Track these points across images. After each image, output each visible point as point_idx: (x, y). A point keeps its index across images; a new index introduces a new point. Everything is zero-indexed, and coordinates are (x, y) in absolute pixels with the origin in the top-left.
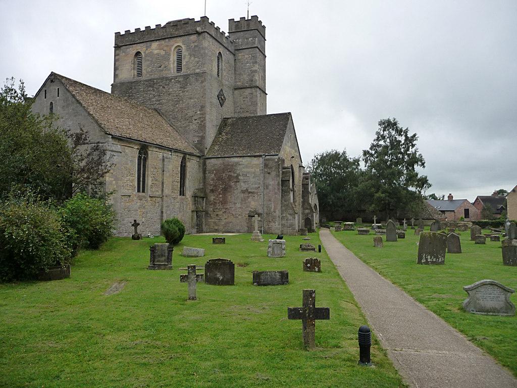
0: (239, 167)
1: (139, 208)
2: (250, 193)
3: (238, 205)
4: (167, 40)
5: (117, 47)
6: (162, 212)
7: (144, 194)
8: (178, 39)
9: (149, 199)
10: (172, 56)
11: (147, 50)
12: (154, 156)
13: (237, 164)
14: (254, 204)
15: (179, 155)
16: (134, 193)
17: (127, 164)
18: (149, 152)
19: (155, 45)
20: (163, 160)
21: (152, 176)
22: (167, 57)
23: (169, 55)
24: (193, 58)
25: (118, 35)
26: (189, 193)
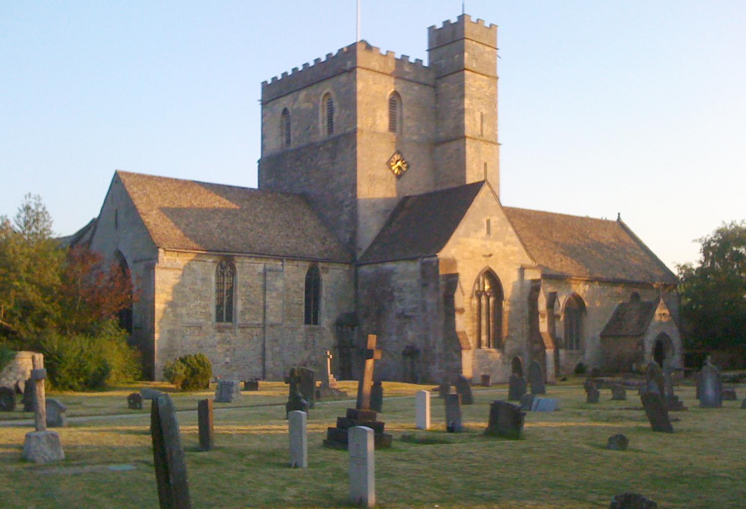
0: (394, 278)
1: (219, 343)
2: (406, 317)
3: (394, 337)
4: (314, 86)
5: (264, 103)
6: (264, 349)
7: (229, 324)
8: (324, 84)
9: (238, 331)
10: (320, 110)
11: (294, 104)
12: (248, 271)
13: (391, 272)
14: (411, 335)
15: (301, 263)
16: (210, 323)
17: (196, 284)
18: (237, 265)
19: (303, 95)
20: (265, 274)
21: (243, 298)
22: (314, 114)
23: (317, 109)
24: (343, 111)
25: (432, 30)
26: (326, 321)
